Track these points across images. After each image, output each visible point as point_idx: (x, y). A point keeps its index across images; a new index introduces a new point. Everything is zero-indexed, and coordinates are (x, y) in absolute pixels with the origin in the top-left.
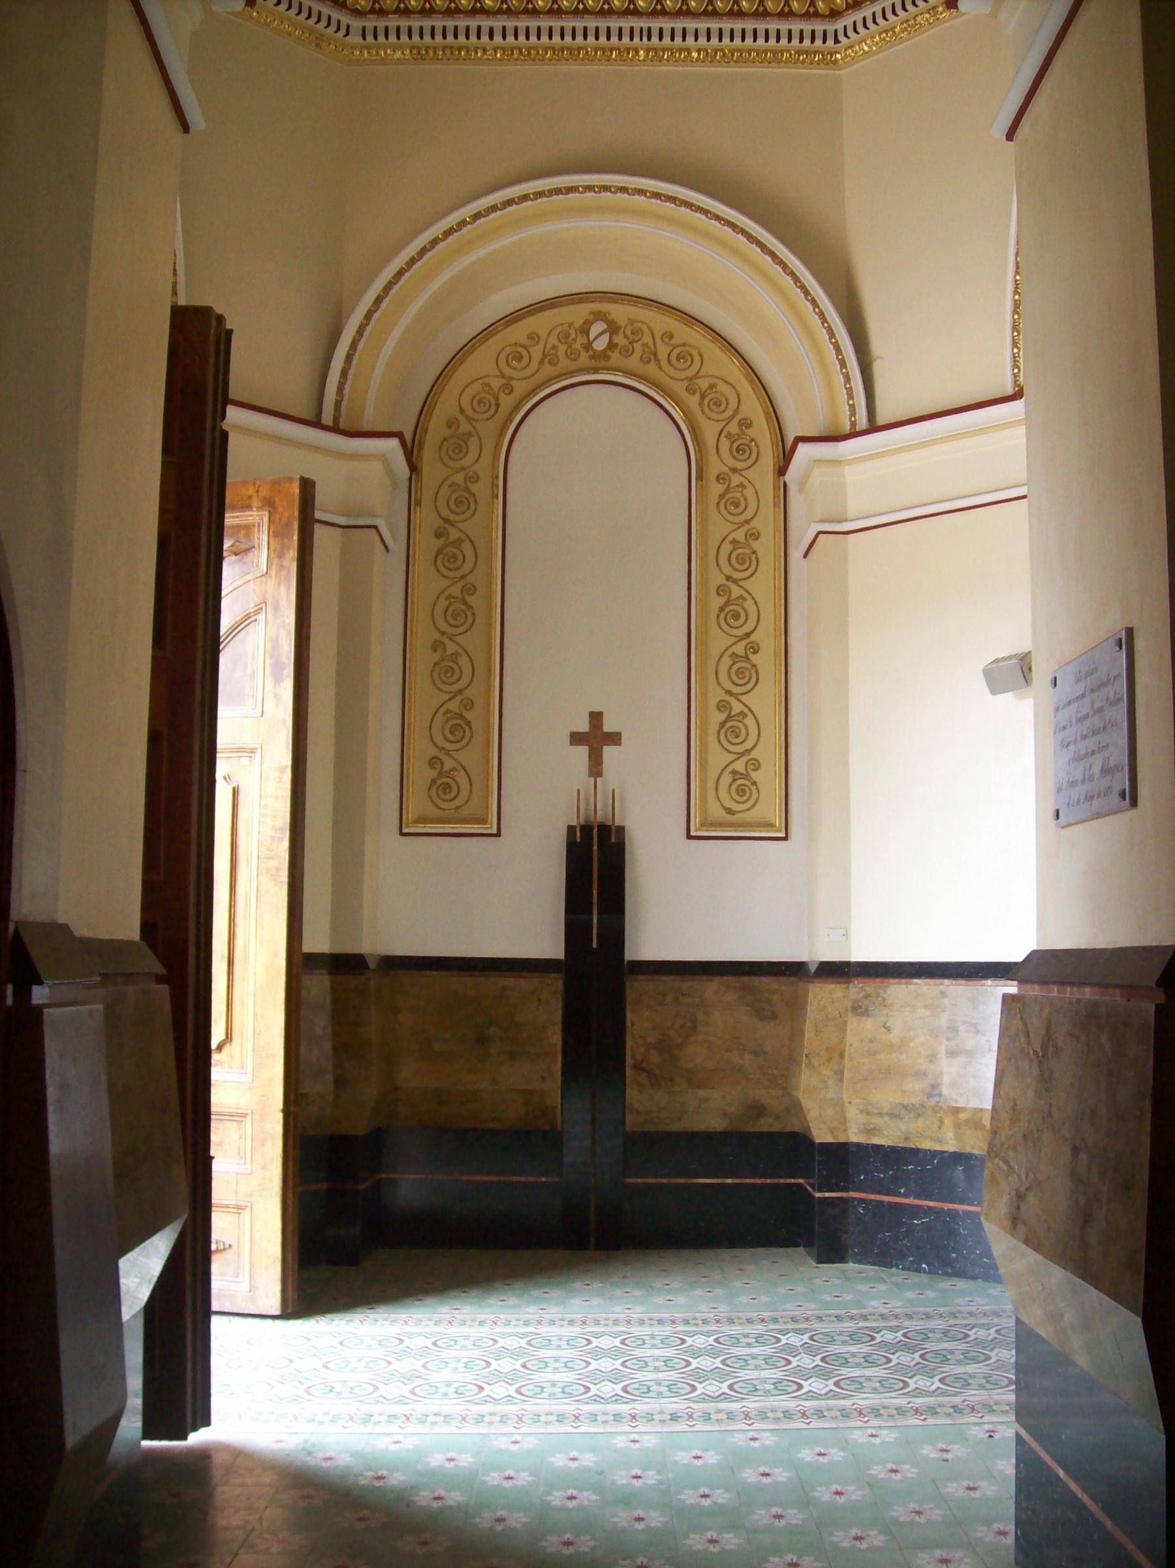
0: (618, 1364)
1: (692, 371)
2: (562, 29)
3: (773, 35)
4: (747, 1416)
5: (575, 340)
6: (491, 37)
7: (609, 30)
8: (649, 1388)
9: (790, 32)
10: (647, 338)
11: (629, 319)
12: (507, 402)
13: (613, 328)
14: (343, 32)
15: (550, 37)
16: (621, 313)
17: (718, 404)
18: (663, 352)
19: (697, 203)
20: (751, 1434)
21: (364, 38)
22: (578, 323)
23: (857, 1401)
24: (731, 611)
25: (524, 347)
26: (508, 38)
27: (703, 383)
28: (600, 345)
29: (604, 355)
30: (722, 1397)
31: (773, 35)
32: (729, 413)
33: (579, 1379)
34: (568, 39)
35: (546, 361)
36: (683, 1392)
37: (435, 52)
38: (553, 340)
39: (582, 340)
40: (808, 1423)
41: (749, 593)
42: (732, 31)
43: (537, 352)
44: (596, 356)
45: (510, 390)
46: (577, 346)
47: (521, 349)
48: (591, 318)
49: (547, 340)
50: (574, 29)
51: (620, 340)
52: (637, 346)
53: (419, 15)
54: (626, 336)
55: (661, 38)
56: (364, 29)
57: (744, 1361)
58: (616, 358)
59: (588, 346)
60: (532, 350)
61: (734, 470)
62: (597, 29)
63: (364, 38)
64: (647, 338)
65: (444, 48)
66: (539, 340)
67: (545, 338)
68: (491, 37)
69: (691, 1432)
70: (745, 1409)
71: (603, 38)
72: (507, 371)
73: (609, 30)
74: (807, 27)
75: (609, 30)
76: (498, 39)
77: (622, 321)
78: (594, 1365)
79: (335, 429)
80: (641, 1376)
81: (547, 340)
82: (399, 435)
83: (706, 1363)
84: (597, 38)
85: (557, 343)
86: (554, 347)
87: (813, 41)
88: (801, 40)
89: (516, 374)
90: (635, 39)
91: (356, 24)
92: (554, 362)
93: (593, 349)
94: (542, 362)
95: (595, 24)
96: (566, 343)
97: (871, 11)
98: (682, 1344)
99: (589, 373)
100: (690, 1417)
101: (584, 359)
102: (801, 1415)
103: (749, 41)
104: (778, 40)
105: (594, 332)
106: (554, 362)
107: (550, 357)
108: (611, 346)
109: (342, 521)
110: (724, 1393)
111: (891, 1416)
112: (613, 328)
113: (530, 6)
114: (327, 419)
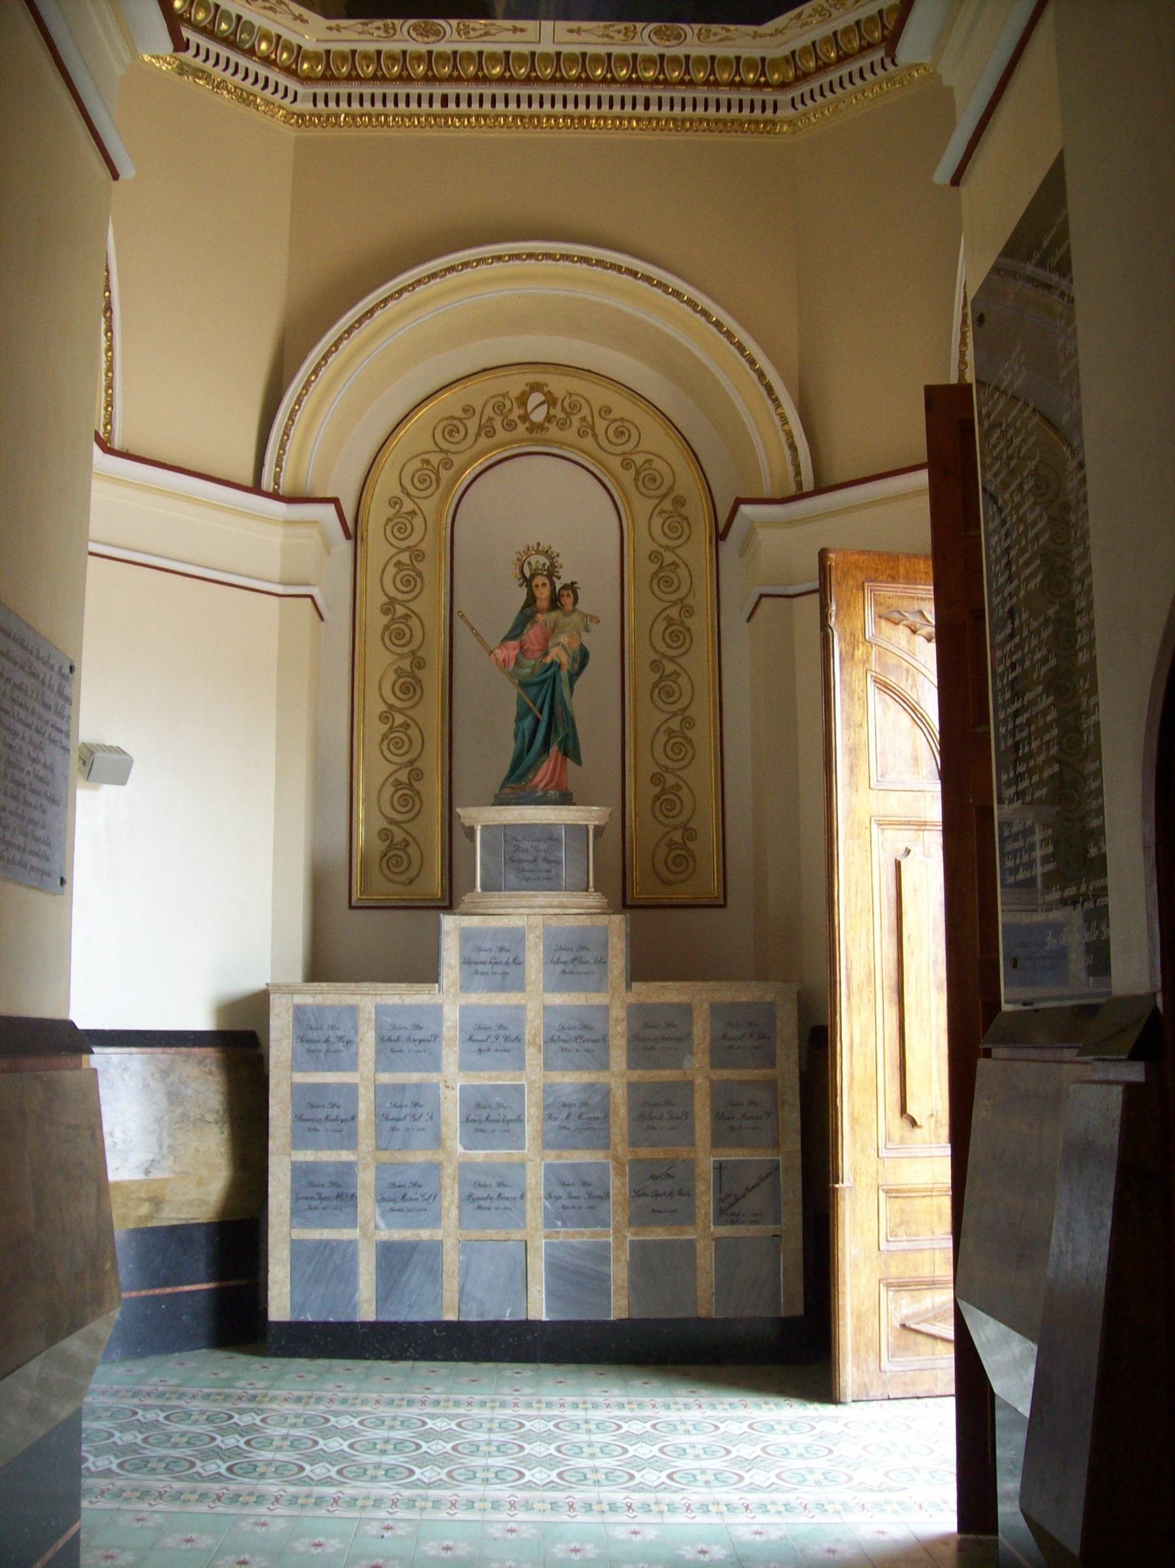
0: (552, 1450)
1: (630, 446)
2: (408, 96)
3: (475, 100)
4: (571, 1506)
5: (511, 410)
6: (493, 104)
7: (634, 99)
8: (585, 1475)
9: (764, 102)
10: (585, 412)
11: (567, 391)
12: (445, 475)
13: (551, 400)
14: (290, 97)
15: (553, 105)
16: (558, 384)
17: (654, 480)
18: (600, 425)
19: (438, 269)
20: (632, 1528)
21: (315, 105)
22: (515, 393)
23: (686, 1495)
24: (664, 687)
25: (460, 420)
26: (434, 105)
27: (639, 459)
28: (538, 416)
29: (540, 427)
30: (550, 1485)
31: (475, 100)
32: (663, 490)
33: (461, 1458)
34: (367, 105)
35: (483, 434)
36: (621, 1480)
37: (588, 122)
38: (489, 412)
39: (517, 412)
40: (573, 1517)
41: (685, 671)
42: (470, 96)
43: (473, 425)
44: (534, 427)
45: (448, 464)
46: (514, 416)
47: (456, 422)
48: (527, 389)
49: (482, 412)
50: (420, 96)
51: (557, 412)
52: (576, 419)
53: (727, 88)
54: (563, 409)
55: (611, 106)
56: (315, 95)
57: (501, 1449)
58: (553, 431)
59: (525, 418)
60: (467, 422)
61: (667, 548)
62: (396, 96)
63: (315, 105)
64: (585, 412)
65: (565, 117)
66: (474, 412)
67: (481, 409)
68: (493, 104)
69: (329, 1518)
70: (570, 1499)
71: (402, 105)
72: (444, 445)
73: (634, 99)
74: (402, 91)
75: (634, 99)
76: (500, 106)
77: (559, 393)
78: (449, 1447)
79: (275, 496)
80: (610, 1463)
81: (482, 412)
82: (335, 501)
83: (644, 1451)
84: (396, 104)
85: (492, 415)
86: (490, 419)
87: (752, 110)
88: (752, 110)
89: (453, 448)
90: (603, 107)
91: (784, 97)
92: (491, 433)
93: (531, 421)
94: (478, 435)
95: (750, 97)
96: (502, 414)
97: (818, 84)
98: (618, 1429)
99: (537, 445)
100: (571, 1506)
101: (521, 428)
102: (568, 1507)
103: (379, 105)
104: (694, 108)
105: (531, 403)
106: (491, 433)
107: (487, 430)
108: (549, 418)
109: (280, 589)
110: (552, 1481)
111: (779, 1512)
112: (551, 400)
113: (712, 78)
114: (267, 483)
